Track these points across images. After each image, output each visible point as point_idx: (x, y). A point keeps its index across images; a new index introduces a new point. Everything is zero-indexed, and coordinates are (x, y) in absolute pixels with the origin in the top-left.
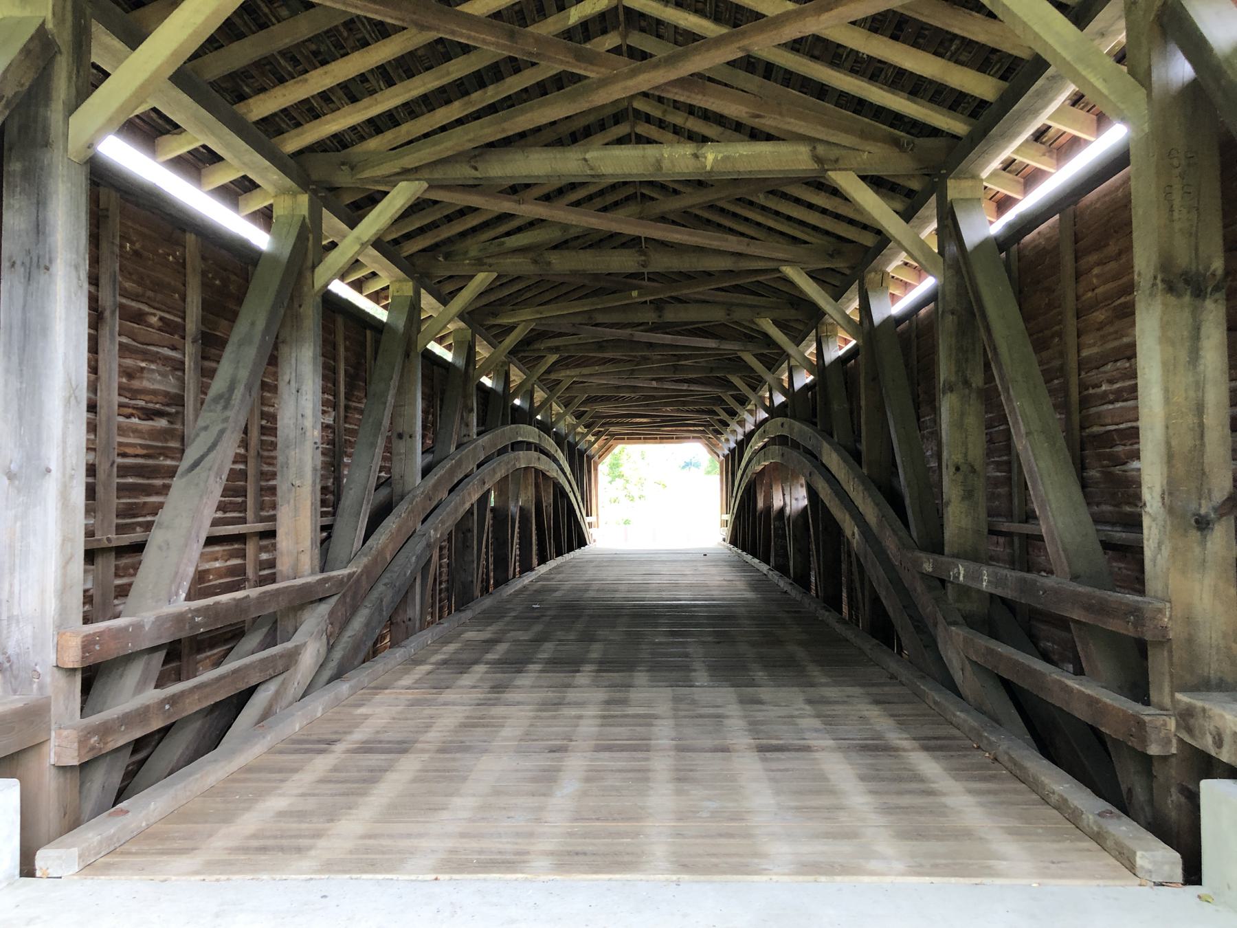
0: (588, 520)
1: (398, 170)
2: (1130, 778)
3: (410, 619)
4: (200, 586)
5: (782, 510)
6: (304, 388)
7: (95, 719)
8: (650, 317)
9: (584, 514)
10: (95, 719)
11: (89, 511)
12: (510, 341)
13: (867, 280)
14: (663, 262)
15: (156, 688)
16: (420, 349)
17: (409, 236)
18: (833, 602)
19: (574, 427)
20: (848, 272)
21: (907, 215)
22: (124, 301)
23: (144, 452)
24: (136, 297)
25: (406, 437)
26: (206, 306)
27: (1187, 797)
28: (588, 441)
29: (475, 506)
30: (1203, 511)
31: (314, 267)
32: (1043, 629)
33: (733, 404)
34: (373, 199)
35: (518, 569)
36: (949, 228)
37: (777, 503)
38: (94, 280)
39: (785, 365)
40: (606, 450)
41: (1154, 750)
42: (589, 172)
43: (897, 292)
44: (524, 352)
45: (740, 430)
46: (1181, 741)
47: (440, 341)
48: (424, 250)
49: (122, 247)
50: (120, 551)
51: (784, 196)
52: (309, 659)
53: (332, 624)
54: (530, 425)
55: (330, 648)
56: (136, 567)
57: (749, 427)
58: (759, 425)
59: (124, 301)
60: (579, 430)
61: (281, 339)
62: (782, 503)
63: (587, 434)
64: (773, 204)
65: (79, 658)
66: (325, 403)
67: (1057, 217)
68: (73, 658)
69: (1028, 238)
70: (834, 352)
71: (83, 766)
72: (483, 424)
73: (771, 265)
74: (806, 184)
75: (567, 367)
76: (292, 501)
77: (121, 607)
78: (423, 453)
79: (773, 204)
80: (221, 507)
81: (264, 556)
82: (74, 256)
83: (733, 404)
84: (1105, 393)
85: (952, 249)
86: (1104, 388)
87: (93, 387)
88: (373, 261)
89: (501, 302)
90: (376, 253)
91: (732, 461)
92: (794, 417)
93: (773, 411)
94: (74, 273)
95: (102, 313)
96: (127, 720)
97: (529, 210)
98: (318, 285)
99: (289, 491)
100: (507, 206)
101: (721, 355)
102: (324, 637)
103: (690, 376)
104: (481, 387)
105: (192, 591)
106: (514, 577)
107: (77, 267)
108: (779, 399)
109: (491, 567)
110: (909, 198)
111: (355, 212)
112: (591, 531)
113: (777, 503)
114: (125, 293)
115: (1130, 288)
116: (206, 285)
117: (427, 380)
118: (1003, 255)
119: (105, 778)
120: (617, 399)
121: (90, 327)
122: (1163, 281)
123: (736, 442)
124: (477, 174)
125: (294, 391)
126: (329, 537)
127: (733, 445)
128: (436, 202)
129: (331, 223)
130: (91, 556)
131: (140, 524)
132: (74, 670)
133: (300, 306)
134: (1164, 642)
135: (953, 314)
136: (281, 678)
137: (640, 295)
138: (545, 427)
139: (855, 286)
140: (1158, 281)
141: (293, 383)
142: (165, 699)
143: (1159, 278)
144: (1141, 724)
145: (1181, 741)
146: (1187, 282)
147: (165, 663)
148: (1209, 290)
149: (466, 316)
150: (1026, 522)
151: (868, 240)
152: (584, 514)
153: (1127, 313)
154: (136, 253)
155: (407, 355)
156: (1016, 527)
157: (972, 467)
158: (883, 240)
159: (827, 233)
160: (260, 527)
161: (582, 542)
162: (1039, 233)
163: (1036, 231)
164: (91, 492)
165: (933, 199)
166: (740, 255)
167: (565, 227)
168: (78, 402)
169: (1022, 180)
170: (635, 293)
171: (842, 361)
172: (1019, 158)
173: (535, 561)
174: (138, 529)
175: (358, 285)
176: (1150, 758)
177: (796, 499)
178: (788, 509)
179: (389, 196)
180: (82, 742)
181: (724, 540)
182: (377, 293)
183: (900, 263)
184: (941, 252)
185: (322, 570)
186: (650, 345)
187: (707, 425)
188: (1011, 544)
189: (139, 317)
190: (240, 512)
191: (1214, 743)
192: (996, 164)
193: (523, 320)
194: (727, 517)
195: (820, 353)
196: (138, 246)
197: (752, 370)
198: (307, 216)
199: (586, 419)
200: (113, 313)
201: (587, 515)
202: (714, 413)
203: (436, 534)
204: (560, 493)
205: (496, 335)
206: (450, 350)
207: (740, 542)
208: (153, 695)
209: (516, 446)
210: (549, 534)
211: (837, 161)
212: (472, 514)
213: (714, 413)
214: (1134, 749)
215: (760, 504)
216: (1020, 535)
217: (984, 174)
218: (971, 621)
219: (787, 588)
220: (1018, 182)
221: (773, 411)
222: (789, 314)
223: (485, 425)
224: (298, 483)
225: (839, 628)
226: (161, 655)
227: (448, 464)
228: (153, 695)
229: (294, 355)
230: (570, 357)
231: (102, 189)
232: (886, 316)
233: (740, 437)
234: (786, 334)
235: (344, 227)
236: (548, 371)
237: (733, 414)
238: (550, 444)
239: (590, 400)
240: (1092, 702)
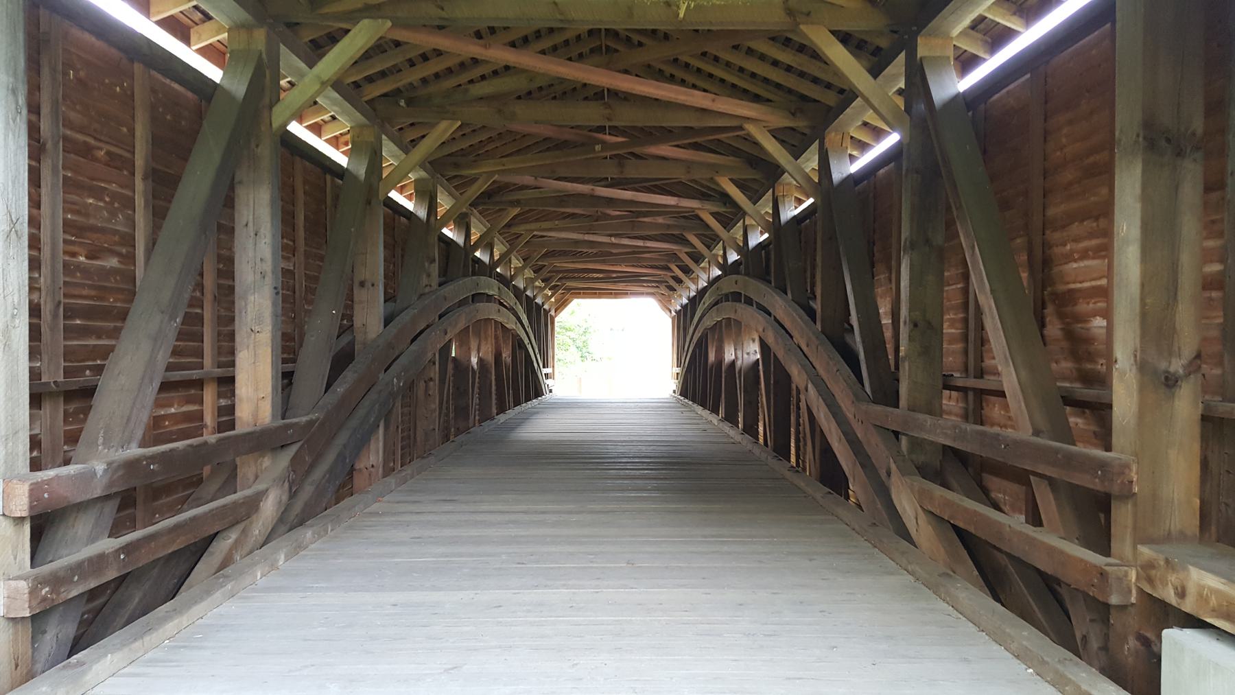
0: (545, 371)
1: (359, 6)
2: (1082, 625)
3: (373, 466)
4: (156, 432)
5: (733, 363)
6: (262, 231)
7: (46, 569)
8: (611, 172)
9: (541, 366)
10: (46, 569)
11: (34, 353)
12: (474, 191)
13: (826, 140)
14: (627, 116)
15: (108, 537)
16: (381, 198)
17: (370, 79)
18: (782, 451)
19: (532, 280)
20: (807, 131)
21: (875, 72)
22: (68, 132)
23: (93, 293)
24: (81, 130)
25: (368, 284)
26: (156, 141)
27: (1143, 644)
28: (544, 298)
29: (437, 355)
30: (1172, 369)
31: (271, 107)
32: (993, 482)
33: (688, 261)
34: (333, 38)
35: (477, 418)
36: (917, 84)
37: (729, 355)
38: (34, 109)
39: (740, 224)
40: (561, 305)
41: (1114, 600)
42: (559, 17)
43: (855, 153)
44: (490, 200)
45: (693, 287)
46: (1141, 591)
47: (401, 190)
48: (385, 95)
49: (65, 74)
50: (69, 396)
51: (750, 51)
52: (269, 508)
53: (294, 471)
54: (491, 277)
55: (293, 495)
56: (86, 411)
57: (703, 284)
58: (712, 283)
59: (68, 132)
60: (537, 284)
61: (236, 180)
62: (733, 357)
63: (544, 288)
64: (738, 60)
65: (26, 507)
66: (284, 248)
67: (1028, 76)
68: (21, 507)
69: (996, 97)
70: (790, 212)
71: (34, 618)
72: (444, 276)
73: (734, 123)
74: (773, 39)
75: (526, 221)
76: (251, 346)
77: (71, 454)
78: (385, 301)
79: (738, 60)
80: (176, 352)
81: (223, 402)
82: (11, 80)
83: (688, 261)
84: (1072, 251)
85: (921, 107)
86: (1068, 247)
87: (34, 222)
88: (331, 103)
89: (463, 153)
90: (336, 95)
91: (683, 320)
92: (747, 274)
93: (725, 267)
94: (11, 98)
95: (44, 145)
96: (81, 569)
97: (499, 55)
98: (275, 125)
99: (249, 337)
100: (474, 49)
101: (678, 213)
102: (286, 485)
103: (650, 233)
104: (444, 240)
105: (147, 438)
106: (474, 425)
107: (14, 92)
108: (733, 257)
109: (452, 415)
110: (875, 56)
111: (316, 50)
112: (549, 382)
113: (729, 355)
114: (68, 124)
115: (1109, 145)
116: (155, 120)
117: (390, 228)
118: (970, 114)
119: (59, 631)
120: (575, 254)
121: (30, 157)
122: (1145, 138)
123: (689, 299)
124: (444, 14)
125: (252, 234)
126: (290, 384)
127: (685, 301)
128: (397, 44)
129: (289, 61)
130: (36, 400)
131: (89, 367)
132: (22, 519)
133: (257, 146)
134: (1128, 495)
135: (917, 172)
136: (240, 527)
137: (603, 150)
138: (505, 281)
139: (816, 145)
140: (1141, 139)
141: (250, 224)
142: (120, 549)
143: (1141, 135)
144: (1103, 574)
145: (1141, 591)
146: (1168, 140)
147: (120, 509)
148: (1188, 151)
149: (428, 165)
150: (982, 377)
151: (830, 99)
152: (541, 366)
153: (1104, 173)
154: (79, 81)
155: (369, 202)
156: (972, 382)
157: (929, 323)
158: (848, 95)
159: (790, 91)
160: (219, 372)
161: (538, 393)
162: (1008, 92)
163: (1004, 91)
164: (35, 333)
165: (902, 56)
166: (704, 110)
167: (530, 74)
168: (19, 237)
169: (990, 40)
170: (598, 148)
171: (797, 220)
172: (990, 16)
173: (494, 411)
174: (88, 372)
175: (317, 129)
176: (1107, 606)
177: (748, 354)
178: (739, 363)
179: (351, 33)
180: (33, 592)
181: (674, 392)
182: (336, 138)
183: (860, 123)
184: (908, 109)
185: (283, 419)
186: (611, 202)
187: (660, 282)
188: (966, 399)
189: (86, 151)
190: (198, 357)
191: (1177, 594)
192: (967, 22)
193: (486, 173)
194: (678, 370)
195: (776, 212)
196: (82, 74)
197: (707, 226)
198: (263, 50)
199: (544, 273)
200: (56, 145)
201: (544, 367)
202: (669, 269)
203: (399, 381)
204: (519, 345)
205: (459, 185)
206: (410, 200)
207: (690, 393)
208: (108, 544)
209: (477, 297)
210: (508, 383)
211: (808, 14)
212: (434, 363)
213: (669, 269)
214: (1094, 599)
215: (712, 357)
216: (974, 390)
217: (956, 32)
218: (925, 472)
219: (738, 438)
220: (986, 42)
221: (725, 267)
222: (749, 174)
223: (446, 276)
224: (257, 328)
225: (788, 474)
226: (115, 503)
227: (411, 312)
228: (108, 544)
229: (251, 196)
230: (531, 210)
231: (42, 11)
232: (845, 175)
233: (693, 294)
234: (744, 194)
235: (303, 65)
236: (508, 225)
237: (687, 271)
238: (510, 299)
239: (549, 255)
240: (1052, 551)
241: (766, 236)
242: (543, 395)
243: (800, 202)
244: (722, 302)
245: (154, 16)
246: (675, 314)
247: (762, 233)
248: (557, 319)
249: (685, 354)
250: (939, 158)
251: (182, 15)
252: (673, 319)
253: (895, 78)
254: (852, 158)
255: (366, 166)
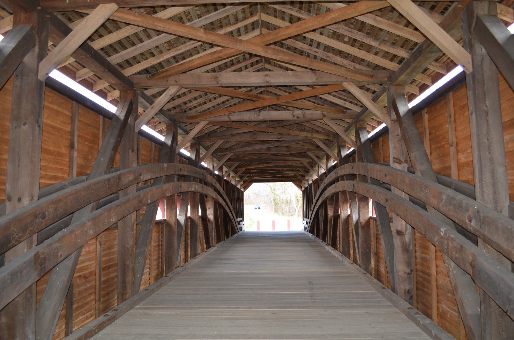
9: (235, 218)
21: (375, 100)
40: (246, 187)
152: (235, 218)
182: (161, 130)
241: (336, 162)
242: (236, 233)
243: (350, 148)
244: (338, 181)
245: (94, 90)
246: (304, 189)
247: (334, 161)
248: (245, 193)
249: (311, 211)
250: (112, 307)
251: (104, 89)
252: (303, 192)
253: (383, 101)
254: (369, 132)
255: (171, 140)
